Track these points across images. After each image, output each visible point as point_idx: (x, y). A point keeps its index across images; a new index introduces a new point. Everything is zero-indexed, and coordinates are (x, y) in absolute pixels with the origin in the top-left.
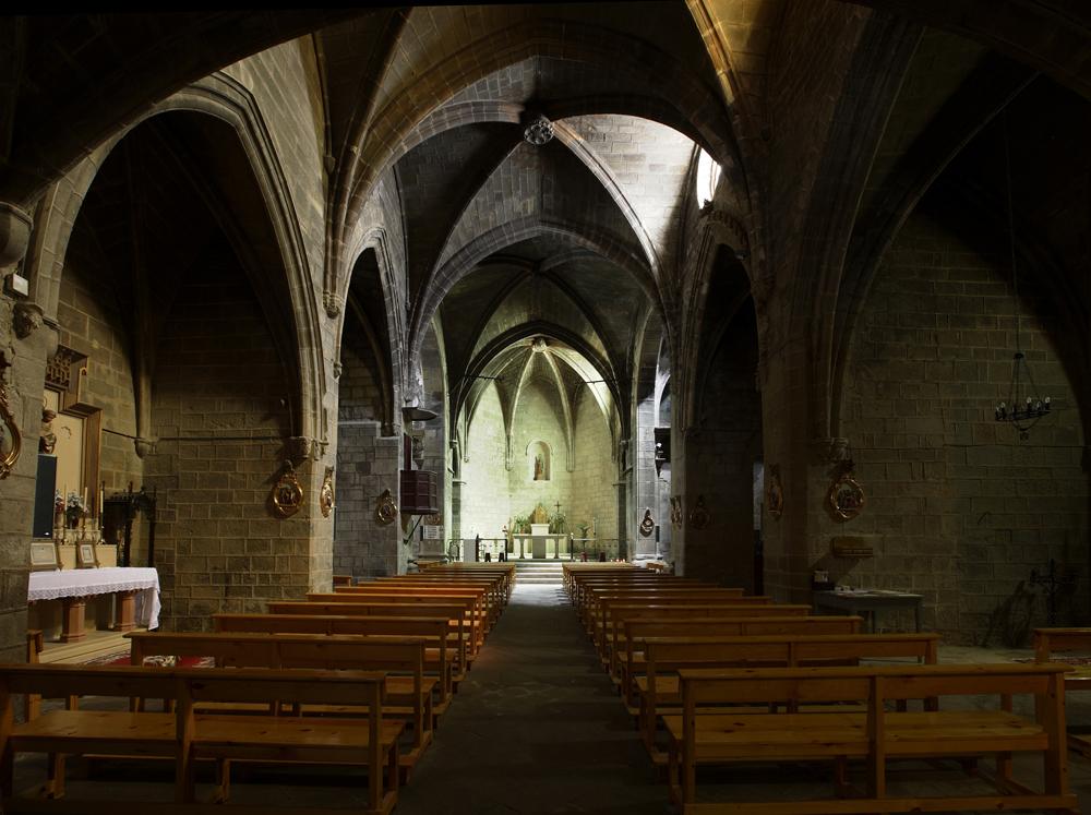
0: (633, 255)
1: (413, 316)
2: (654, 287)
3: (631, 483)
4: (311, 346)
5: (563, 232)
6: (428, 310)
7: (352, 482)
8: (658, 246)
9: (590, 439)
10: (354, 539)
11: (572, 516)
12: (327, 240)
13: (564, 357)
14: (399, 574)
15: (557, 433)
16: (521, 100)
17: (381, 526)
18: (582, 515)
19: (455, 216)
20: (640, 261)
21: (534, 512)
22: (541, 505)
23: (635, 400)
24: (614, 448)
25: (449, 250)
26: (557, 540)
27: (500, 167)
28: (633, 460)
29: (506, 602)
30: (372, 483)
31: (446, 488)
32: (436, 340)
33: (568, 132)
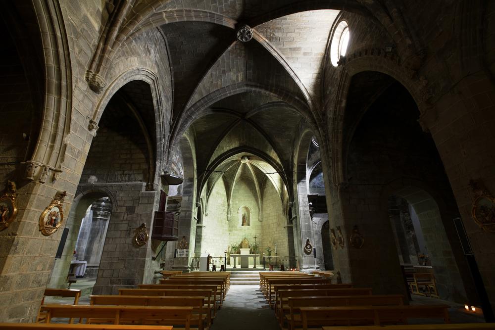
0: (296, 98)
1: (173, 128)
2: (310, 113)
3: (296, 224)
4: (59, 93)
5: (258, 90)
6: (183, 125)
7: (122, 218)
8: (310, 91)
9: (271, 204)
10: (116, 256)
11: (262, 244)
12: (99, 45)
13: (256, 165)
14: (144, 283)
15: (254, 203)
16: (236, 17)
17: (136, 248)
18: (267, 244)
19: (200, 78)
20: (300, 100)
21: (242, 242)
22: (245, 238)
23: (296, 181)
24: (283, 208)
25: (195, 97)
26: (255, 257)
27: (224, 54)
28: (297, 212)
29: (220, 307)
30: (135, 219)
31: (192, 228)
32: (191, 152)
33: (258, 34)
